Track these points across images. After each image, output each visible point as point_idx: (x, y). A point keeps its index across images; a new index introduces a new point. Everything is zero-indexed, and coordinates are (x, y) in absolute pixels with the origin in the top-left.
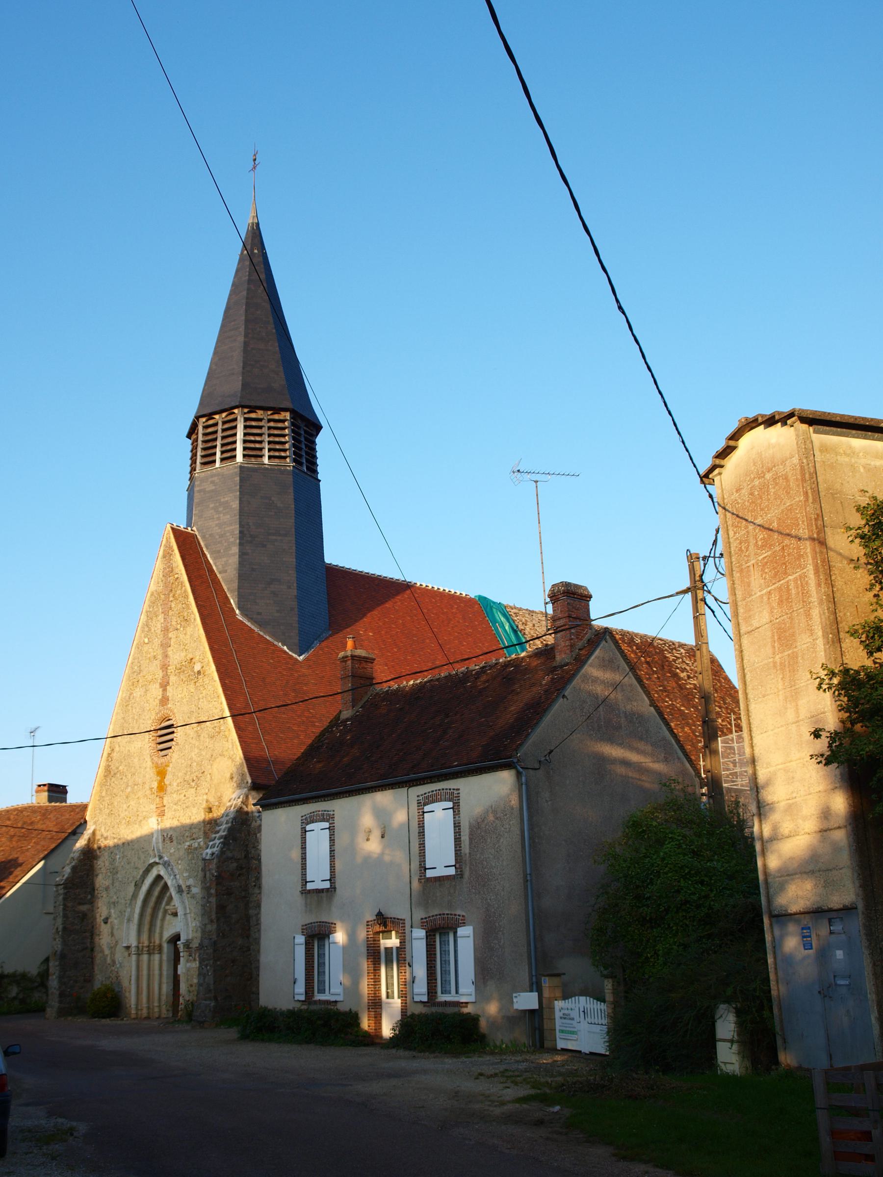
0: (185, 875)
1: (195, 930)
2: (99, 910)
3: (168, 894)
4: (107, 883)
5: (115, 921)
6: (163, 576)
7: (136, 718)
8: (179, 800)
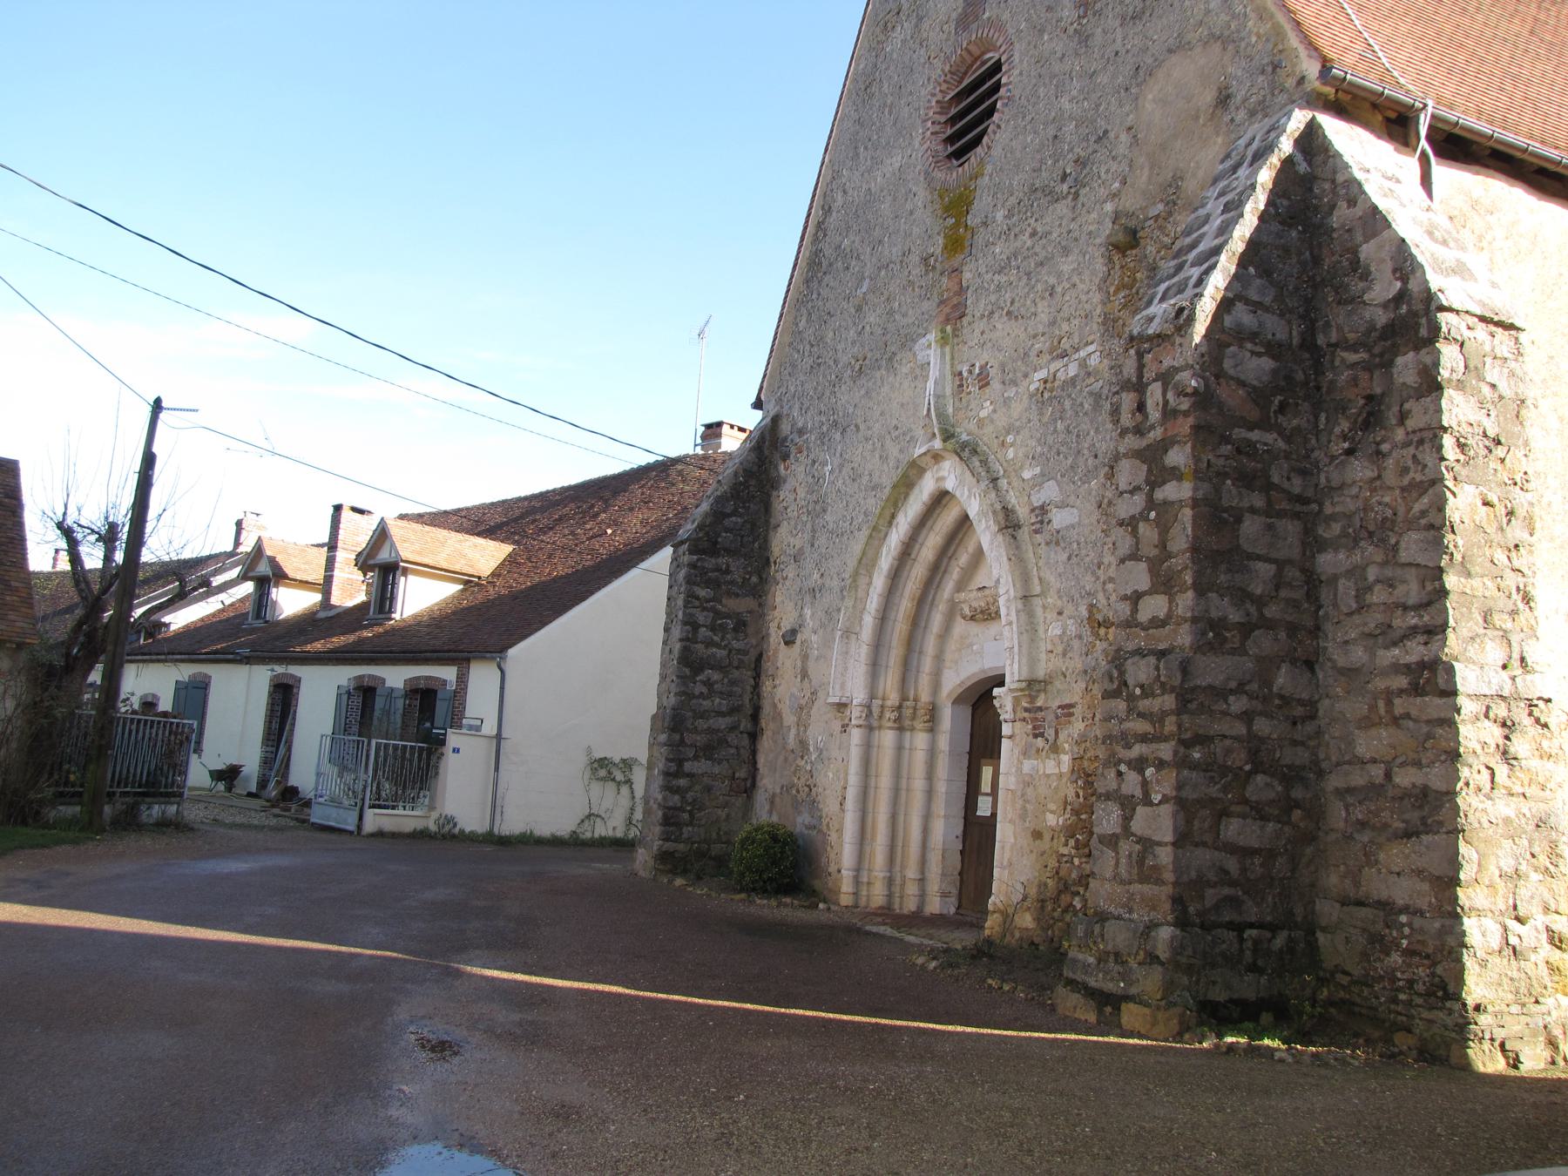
1: (1060, 649)
2: (776, 613)
3: (971, 547)
4: (797, 542)
5: (814, 638)
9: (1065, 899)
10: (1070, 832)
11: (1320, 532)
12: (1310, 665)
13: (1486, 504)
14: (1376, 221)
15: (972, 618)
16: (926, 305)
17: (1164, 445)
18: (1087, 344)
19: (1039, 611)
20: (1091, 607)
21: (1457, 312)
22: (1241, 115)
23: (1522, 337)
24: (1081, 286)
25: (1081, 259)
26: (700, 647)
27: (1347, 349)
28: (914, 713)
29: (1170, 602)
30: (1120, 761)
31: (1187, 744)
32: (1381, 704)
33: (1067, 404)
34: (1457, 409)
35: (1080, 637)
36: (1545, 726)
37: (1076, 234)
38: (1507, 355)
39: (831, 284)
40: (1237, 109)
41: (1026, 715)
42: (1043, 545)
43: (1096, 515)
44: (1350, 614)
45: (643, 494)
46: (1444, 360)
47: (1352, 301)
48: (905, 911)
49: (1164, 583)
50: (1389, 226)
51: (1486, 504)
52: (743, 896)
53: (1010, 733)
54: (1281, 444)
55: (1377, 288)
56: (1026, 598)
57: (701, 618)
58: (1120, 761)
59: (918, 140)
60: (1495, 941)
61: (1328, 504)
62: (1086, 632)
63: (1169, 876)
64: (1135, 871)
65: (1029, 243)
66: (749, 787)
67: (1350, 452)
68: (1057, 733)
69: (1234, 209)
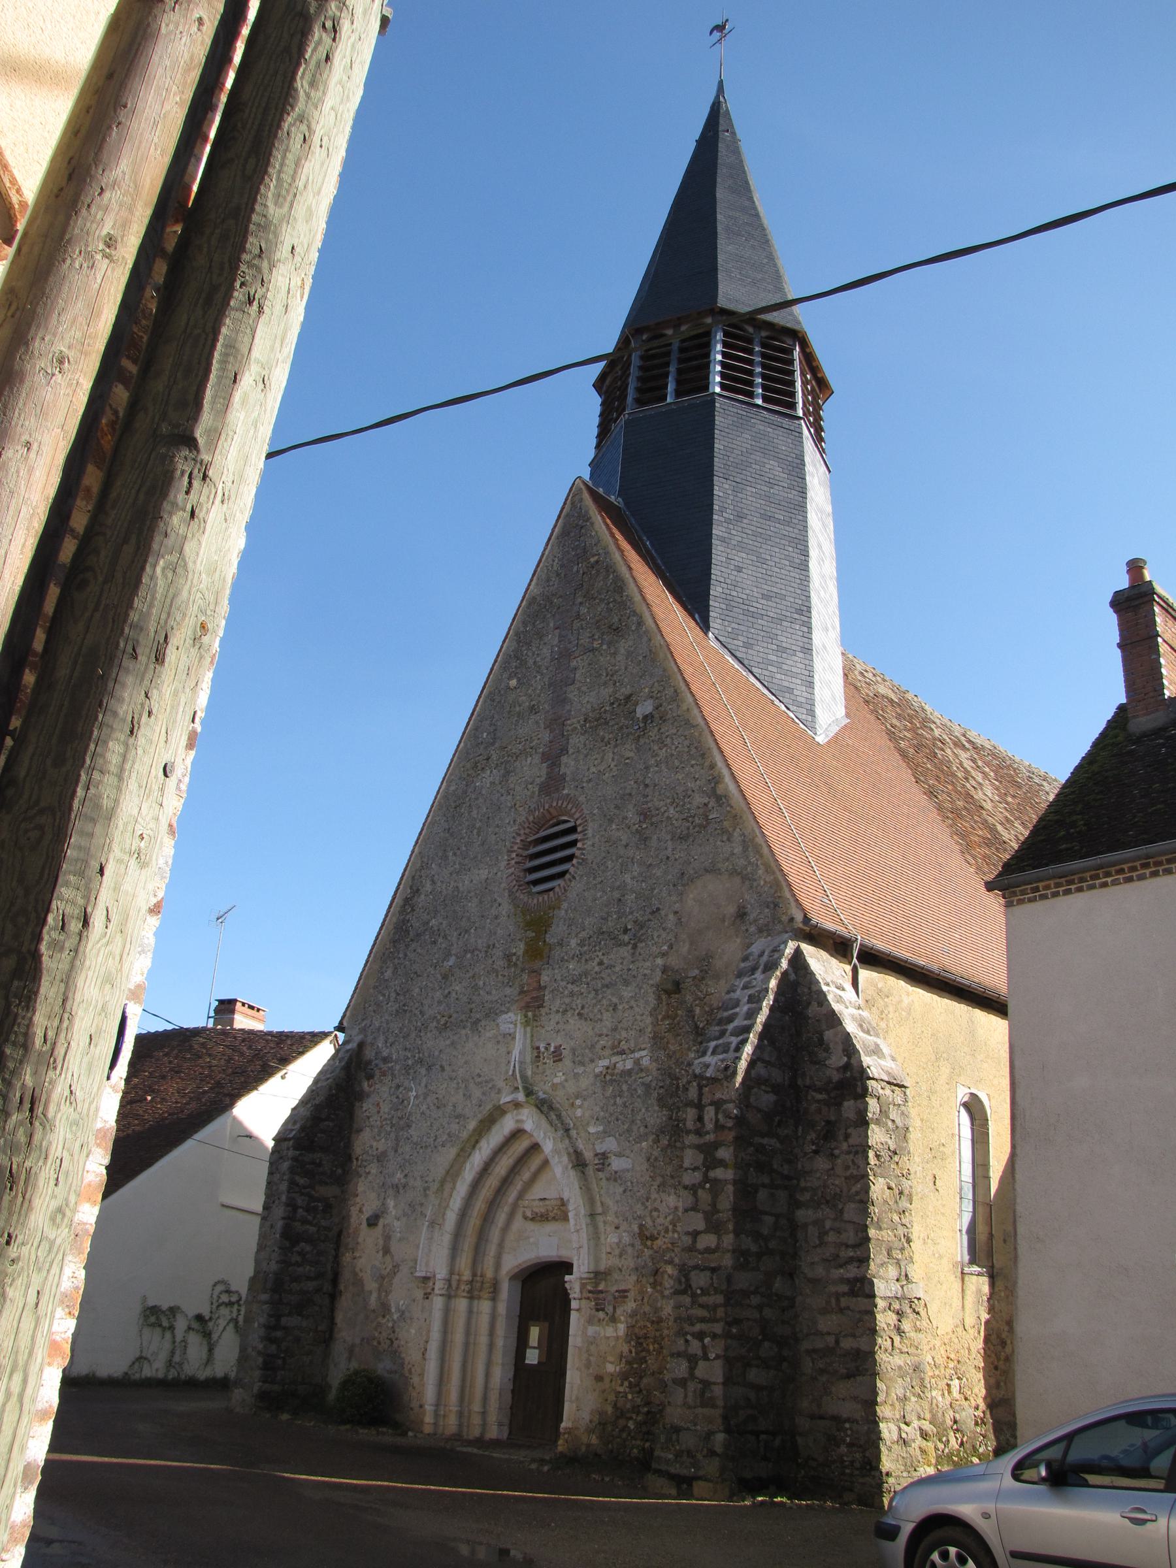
0: (592, 1130)
1: (617, 1252)
2: (358, 1200)
4: (381, 1145)
5: (396, 1224)
6: (562, 566)
7: (477, 825)
8: (586, 974)
9: (622, 1422)
10: (624, 1376)
11: (798, 1197)
12: (791, 1275)
13: (889, 1188)
14: (834, 1019)
15: (532, 1219)
16: (508, 991)
17: (716, 1145)
18: (641, 1049)
19: (601, 1225)
20: (641, 1226)
21: (876, 1080)
22: (753, 929)
23: (908, 1091)
24: (637, 1009)
25: (637, 991)
26: (297, 1224)
27: (815, 1090)
28: (482, 1286)
29: (719, 1239)
30: (687, 1333)
31: (729, 1324)
32: (833, 1301)
33: (625, 1087)
34: (877, 1136)
35: (633, 1245)
36: (918, 1313)
37: (635, 973)
38: (901, 1102)
39: (419, 951)
40: (751, 924)
41: (590, 1295)
42: (604, 1180)
43: (645, 1166)
44: (815, 1247)
45: (170, 1062)
46: (870, 1108)
47: (816, 1063)
48: (471, 1437)
49: (714, 1227)
50: (841, 1024)
51: (889, 1188)
52: (348, 1427)
53: (577, 1307)
54: (778, 1145)
55: (834, 1058)
56: (592, 1215)
57: (300, 1201)
58: (687, 1333)
59: (503, 864)
60: (895, 1437)
61: (802, 1180)
62: (638, 1242)
63: (720, 1403)
64: (698, 1401)
65: (597, 969)
66: (327, 1338)
67: (816, 1152)
68: (615, 1308)
69: (756, 1000)
